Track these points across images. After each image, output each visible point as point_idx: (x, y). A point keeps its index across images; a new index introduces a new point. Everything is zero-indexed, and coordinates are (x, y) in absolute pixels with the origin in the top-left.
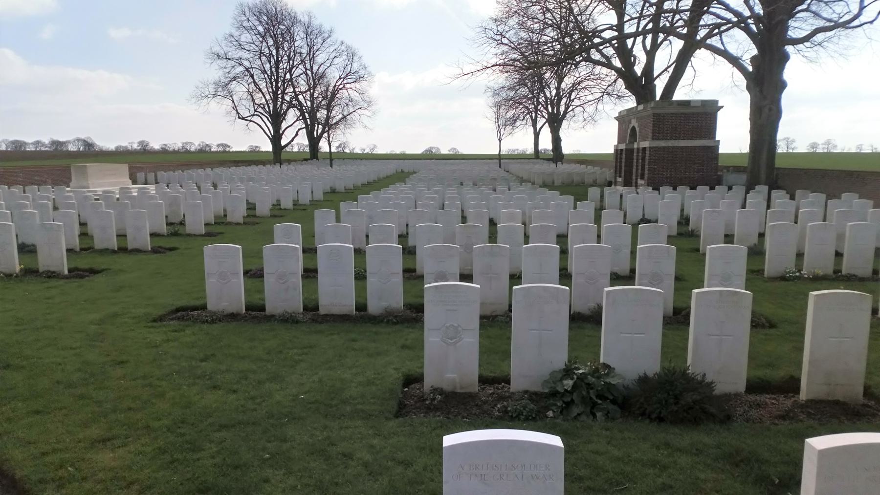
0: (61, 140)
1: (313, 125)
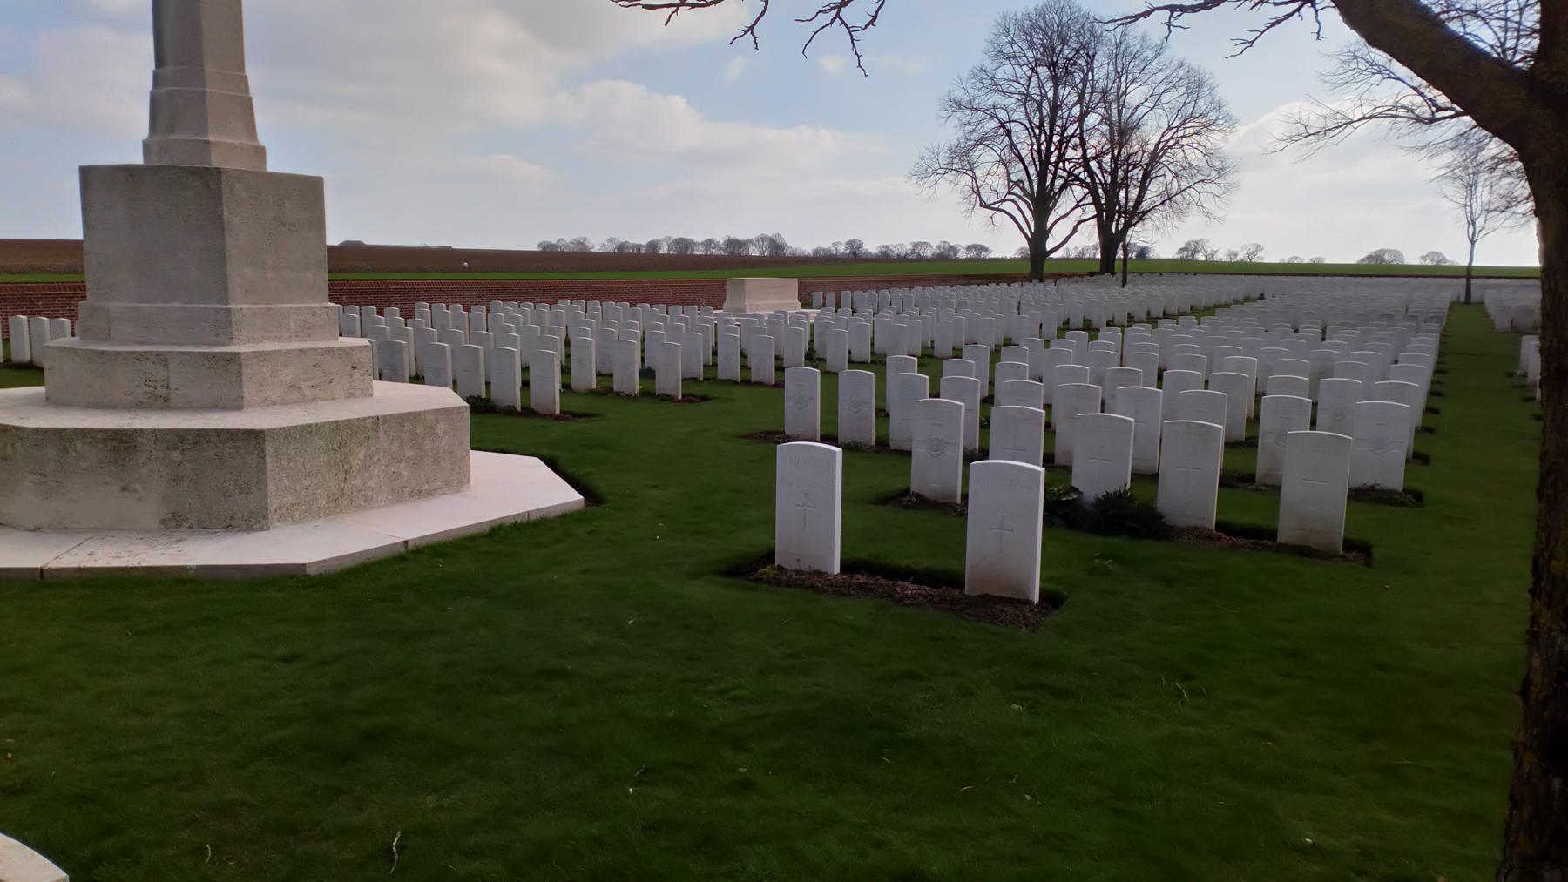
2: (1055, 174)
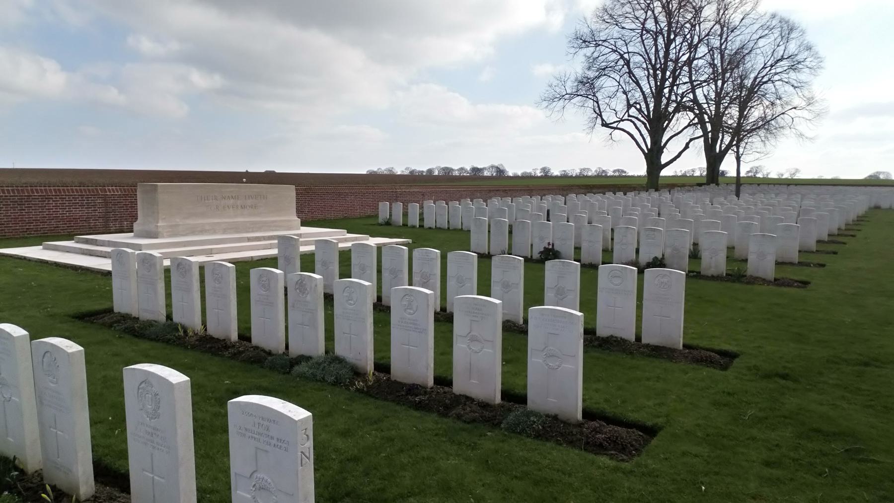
1: (715, 132)
2: (669, 99)
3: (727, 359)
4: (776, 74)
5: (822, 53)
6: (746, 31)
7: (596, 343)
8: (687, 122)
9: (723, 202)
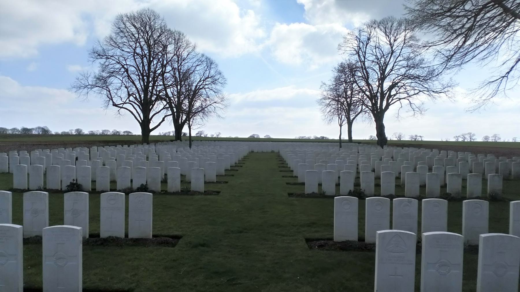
0: (28, 128)
3: (176, 240)
4: (206, 85)
5: (226, 77)
6: (190, 61)
7: (99, 243)
8: (162, 107)
9: (182, 149)
